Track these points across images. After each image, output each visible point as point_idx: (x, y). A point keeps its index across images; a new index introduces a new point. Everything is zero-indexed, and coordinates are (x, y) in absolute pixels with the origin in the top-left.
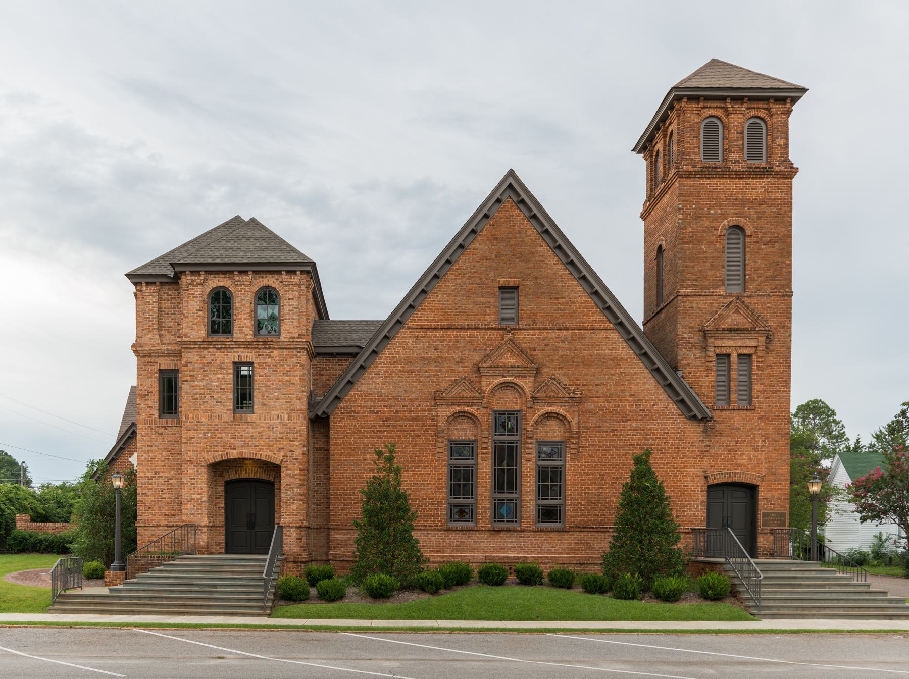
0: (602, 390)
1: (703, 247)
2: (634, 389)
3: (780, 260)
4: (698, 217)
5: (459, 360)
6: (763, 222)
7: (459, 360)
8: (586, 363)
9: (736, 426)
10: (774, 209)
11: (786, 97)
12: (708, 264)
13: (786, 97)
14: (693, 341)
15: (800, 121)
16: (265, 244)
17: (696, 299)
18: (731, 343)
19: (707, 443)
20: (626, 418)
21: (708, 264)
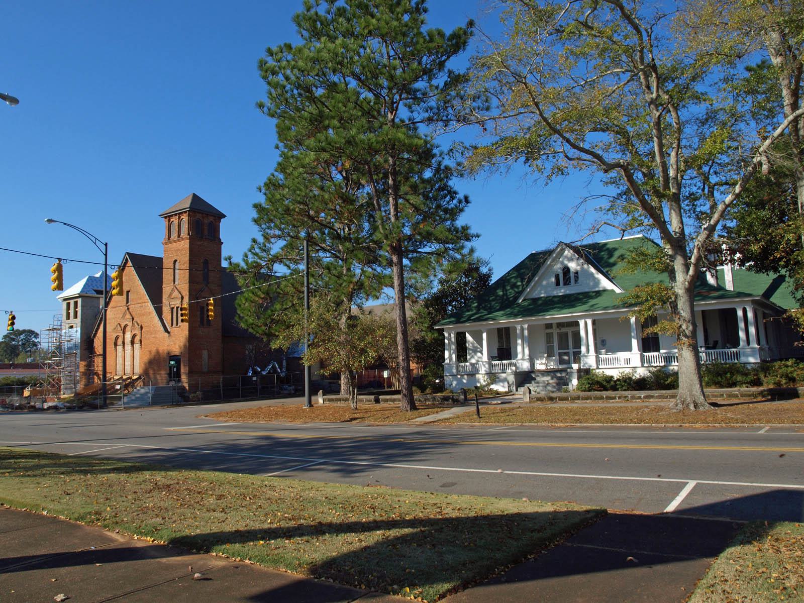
8: (143, 315)
11: (224, 216)
13: (224, 216)
15: (223, 223)
20: (152, 334)
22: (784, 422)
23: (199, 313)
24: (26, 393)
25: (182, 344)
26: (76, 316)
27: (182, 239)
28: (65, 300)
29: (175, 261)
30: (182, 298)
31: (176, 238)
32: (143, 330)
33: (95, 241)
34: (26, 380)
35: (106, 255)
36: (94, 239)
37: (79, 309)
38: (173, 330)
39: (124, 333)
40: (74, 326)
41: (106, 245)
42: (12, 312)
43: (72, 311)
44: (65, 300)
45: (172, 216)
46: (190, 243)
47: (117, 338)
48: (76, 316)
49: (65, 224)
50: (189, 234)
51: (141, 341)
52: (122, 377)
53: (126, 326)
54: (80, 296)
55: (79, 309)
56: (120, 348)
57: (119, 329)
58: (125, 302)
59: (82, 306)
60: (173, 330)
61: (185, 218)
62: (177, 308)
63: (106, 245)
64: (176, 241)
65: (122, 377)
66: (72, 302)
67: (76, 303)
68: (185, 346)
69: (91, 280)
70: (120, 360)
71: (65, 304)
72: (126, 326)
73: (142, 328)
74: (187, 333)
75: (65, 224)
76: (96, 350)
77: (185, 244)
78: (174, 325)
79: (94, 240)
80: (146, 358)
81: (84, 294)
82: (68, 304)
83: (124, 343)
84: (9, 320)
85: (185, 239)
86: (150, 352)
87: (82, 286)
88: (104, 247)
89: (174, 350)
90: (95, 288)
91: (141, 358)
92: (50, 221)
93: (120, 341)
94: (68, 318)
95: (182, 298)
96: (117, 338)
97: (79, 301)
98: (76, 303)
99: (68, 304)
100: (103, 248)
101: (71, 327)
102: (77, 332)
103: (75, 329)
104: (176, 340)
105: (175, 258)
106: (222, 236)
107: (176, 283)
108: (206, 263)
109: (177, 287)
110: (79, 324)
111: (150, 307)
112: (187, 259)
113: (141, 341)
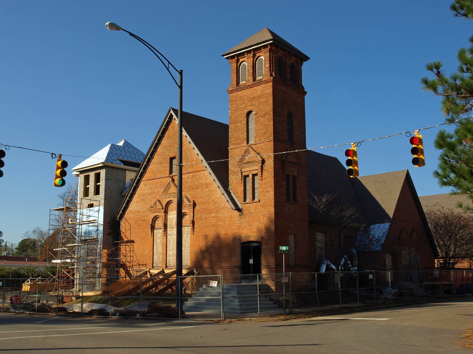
0: (202, 199)
1: (238, 124)
2: (213, 198)
3: (268, 123)
4: (236, 110)
5: (157, 192)
6: (261, 106)
7: (157, 192)
8: (197, 188)
9: (252, 211)
10: (265, 99)
11: (306, 58)
12: (240, 132)
13: (306, 58)
14: (235, 170)
15: (305, 66)
16: (305, 204)
17: (236, 150)
18: (248, 169)
19: (240, 221)
20: (210, 212)
21: (240, 132)
22: (180, 315)
23: (284, 183)
24: (26, 287)
25: (262, 226)
26: (97, 192)
27: (261, 82)
28: (82, 172)
29: (250, 112)
30: (263, 162)
31: (251, 82)
32: (197, 208)
33: (168, 65)
34: (22, 272)
35: (181, 87)
36: (166, 63)
37: (102, 184)
38: (249, 207)
39: (166, 212)
40: (95, 203)
41: (181, 73)
42: (60, 156)
43: (91, 186)
44: (82, 172)
45: (243, 54)
46: (274, 87)
47: (155, 219)
48: (97, 192)
49: (131, 34)
50: (271, 75)
51: (193, 223)
52: (163, 272)
53: (169, 203)
54: (104, 166)
55: (102, 184)
56: (159, 233)
57: (159, 206)
58: (168, 172)
59: (107, 179)
60: (249, 207)
61: (264, 57)
62: (254, 175)
63: (181, 73)
64: (251, 86)
65: (163, 272)
66: (92, 175)
67: (98, 178)
68: (268, 229)
69: (114, 148)
70: (158, 249)
71: (82, 177)
72: (169, 203)
73: (195, 205)
74: (272, 210)
75: (131, 34)
76: (122, 235)
77: (267, 89)
78: (248, 200)
79: (166, 63)
80: (201, 244)
81: (110, 164)
82: (87, 179)
83: (165, 226)
84: (58, 168)
85: (266, 82)
86: (206, 237)
87: (106, 155)
88: (179, 76)
89: (250, 234)
90: (121, 158)
91: (191, 245)
92: (113, 26)
93: (159, 223)
94: (86, 193)
95: (263, 162)
96: (155, 219)
97: (103, 173)
98: (98, 178)
99: (87, 179)
100: (177, 77)
101: (91, 206)
102: (98, 211)
103: (96, 209)
104: (255, 219)
105: (249, 109)
106: (305, 83)
107: (250, 142)
108: (290, 115)
109: (254, 148)
110: (102, 202)
111: (209, 176)
112: (269, 107)
113: (193, 223)
